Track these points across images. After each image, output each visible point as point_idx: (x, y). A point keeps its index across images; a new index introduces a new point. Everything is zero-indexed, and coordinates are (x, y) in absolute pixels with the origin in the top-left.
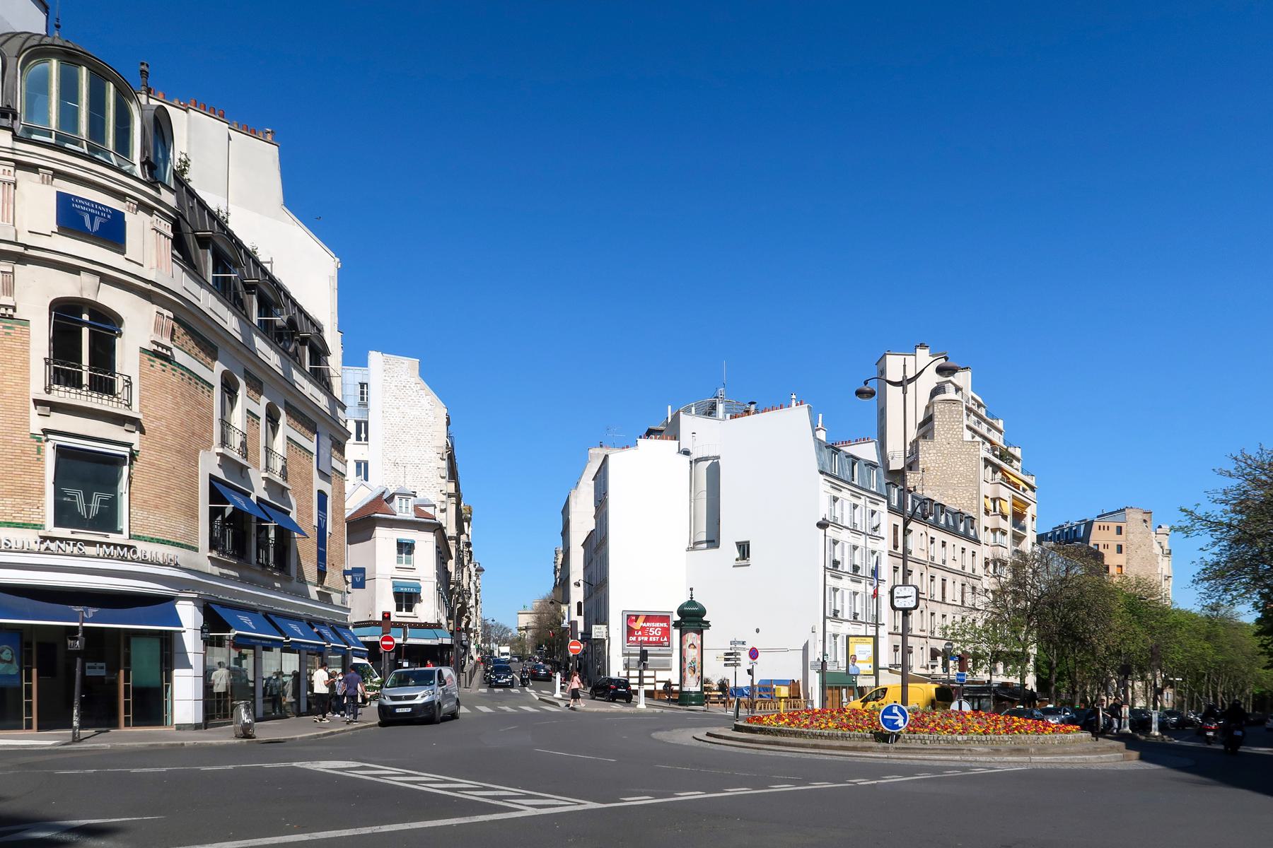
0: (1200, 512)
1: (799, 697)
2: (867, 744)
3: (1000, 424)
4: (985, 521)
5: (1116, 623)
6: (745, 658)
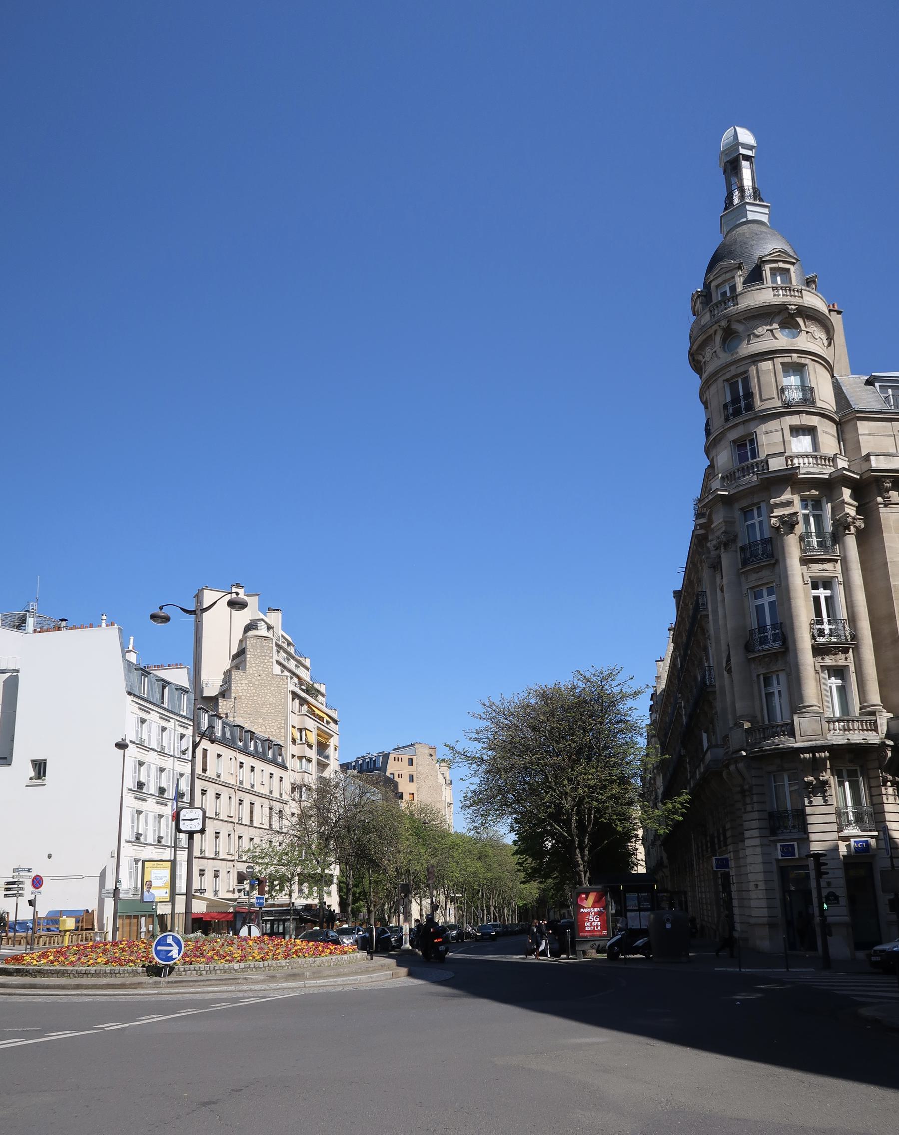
0: (459, 748)
1: (93, 929)
2: (137, 979)
3: (307, 662)
4: (291, 749)
5: (404, 845)
6: (28, 890)
